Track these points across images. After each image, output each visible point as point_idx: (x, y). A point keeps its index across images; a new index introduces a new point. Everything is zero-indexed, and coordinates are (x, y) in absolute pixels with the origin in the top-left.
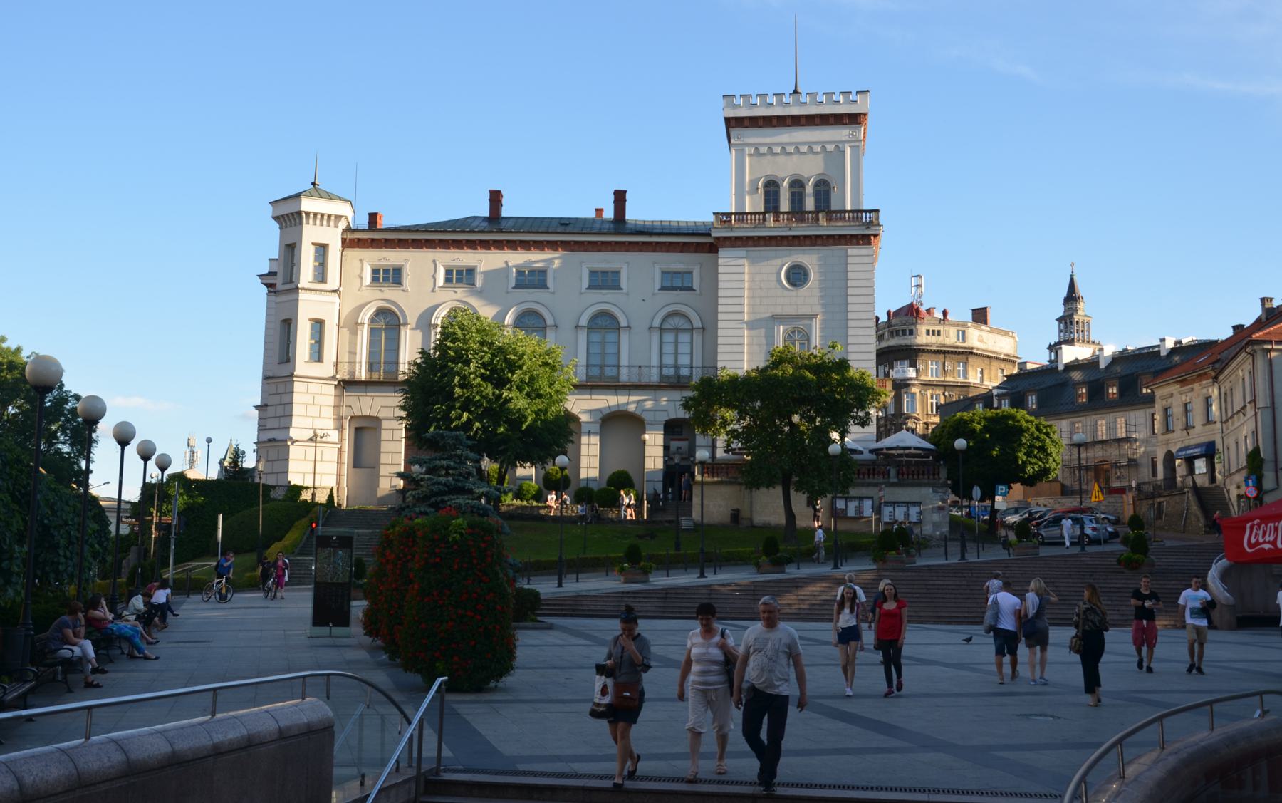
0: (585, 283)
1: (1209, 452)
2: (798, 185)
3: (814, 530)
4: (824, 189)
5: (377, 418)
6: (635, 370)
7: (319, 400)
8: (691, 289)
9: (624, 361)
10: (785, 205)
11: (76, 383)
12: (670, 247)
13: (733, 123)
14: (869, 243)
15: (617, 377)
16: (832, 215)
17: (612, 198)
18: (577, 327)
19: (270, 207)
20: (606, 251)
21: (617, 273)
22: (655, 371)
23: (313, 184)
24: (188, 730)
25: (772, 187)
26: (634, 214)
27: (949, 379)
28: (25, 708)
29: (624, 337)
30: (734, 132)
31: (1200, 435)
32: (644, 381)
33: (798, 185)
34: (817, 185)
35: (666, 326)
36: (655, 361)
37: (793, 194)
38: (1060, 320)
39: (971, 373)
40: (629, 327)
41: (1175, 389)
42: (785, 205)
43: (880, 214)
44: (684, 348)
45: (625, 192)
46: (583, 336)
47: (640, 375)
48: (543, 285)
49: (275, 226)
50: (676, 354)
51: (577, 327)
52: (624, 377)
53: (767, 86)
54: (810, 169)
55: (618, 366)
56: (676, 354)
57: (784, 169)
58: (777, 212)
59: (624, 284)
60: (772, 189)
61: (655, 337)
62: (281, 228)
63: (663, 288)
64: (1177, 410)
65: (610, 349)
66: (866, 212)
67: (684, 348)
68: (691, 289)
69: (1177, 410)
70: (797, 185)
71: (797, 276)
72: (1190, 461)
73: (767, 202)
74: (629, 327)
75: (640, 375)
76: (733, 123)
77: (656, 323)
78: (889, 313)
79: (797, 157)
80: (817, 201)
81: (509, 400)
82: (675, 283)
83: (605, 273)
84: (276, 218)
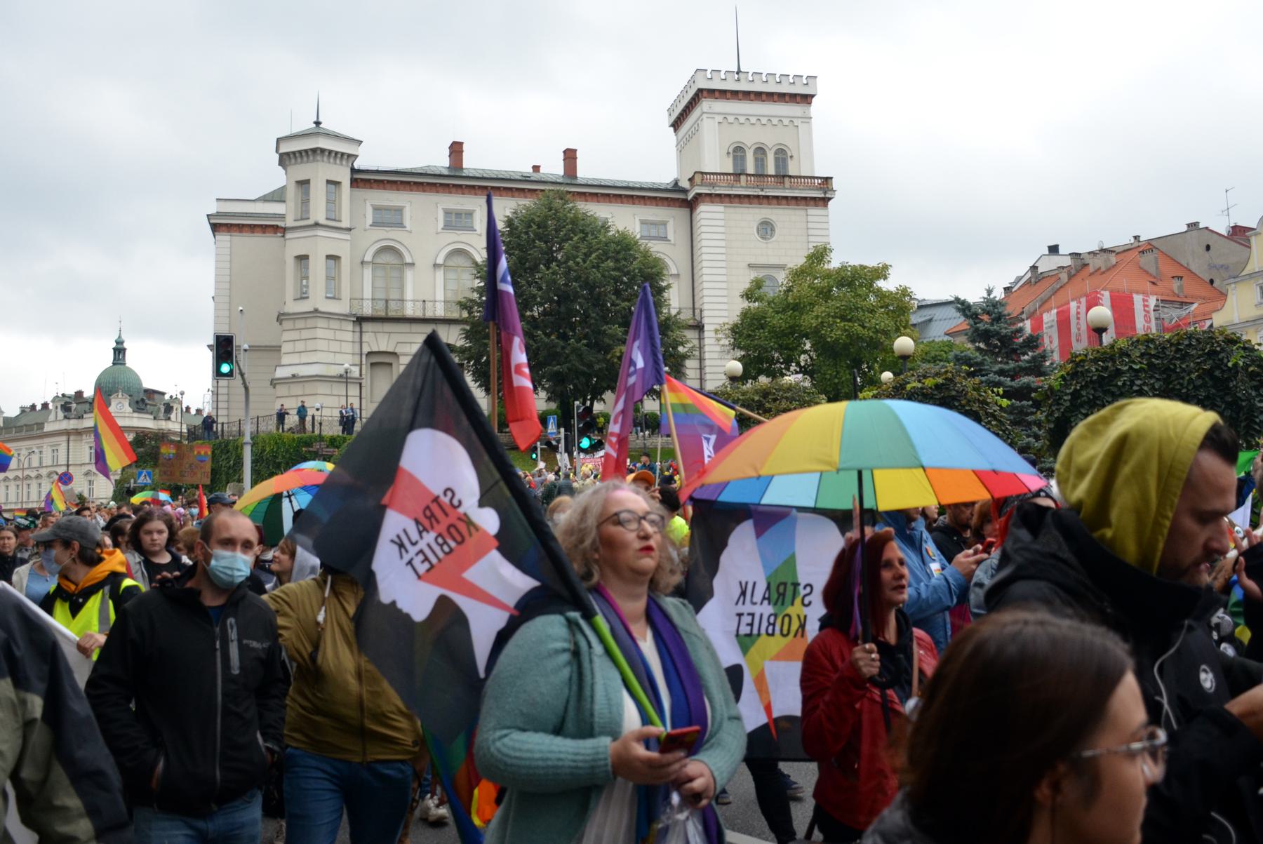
0: (441, 224)
3: (1047, 431)
4: (782, 156)
5: (394, 354)
7: (340, 335)
8: (665, 239)
9: (409, 295)
12: (643, 200)
16: (782, 177)
17: (562, 156)
18: (363, 263)
20: (431, 191)
24: (1064, 546)
25: (738, 152)
26: (585, 171)
29: (409, 274)
32: (429, 314)
45: (461, 144)
46: (368, 272)
47: (424, 309)
51: (363, 263)
54: (770, 139)
55: (402, 300)
57: (750, 138)
59: (407, 222)
60: (780, 156)
65: (380, 283)
68: (665, 239)
70: (760, 151)
71: (766, 229)
73: (735, 165)
75: (424, 309)
79: (759, 127)
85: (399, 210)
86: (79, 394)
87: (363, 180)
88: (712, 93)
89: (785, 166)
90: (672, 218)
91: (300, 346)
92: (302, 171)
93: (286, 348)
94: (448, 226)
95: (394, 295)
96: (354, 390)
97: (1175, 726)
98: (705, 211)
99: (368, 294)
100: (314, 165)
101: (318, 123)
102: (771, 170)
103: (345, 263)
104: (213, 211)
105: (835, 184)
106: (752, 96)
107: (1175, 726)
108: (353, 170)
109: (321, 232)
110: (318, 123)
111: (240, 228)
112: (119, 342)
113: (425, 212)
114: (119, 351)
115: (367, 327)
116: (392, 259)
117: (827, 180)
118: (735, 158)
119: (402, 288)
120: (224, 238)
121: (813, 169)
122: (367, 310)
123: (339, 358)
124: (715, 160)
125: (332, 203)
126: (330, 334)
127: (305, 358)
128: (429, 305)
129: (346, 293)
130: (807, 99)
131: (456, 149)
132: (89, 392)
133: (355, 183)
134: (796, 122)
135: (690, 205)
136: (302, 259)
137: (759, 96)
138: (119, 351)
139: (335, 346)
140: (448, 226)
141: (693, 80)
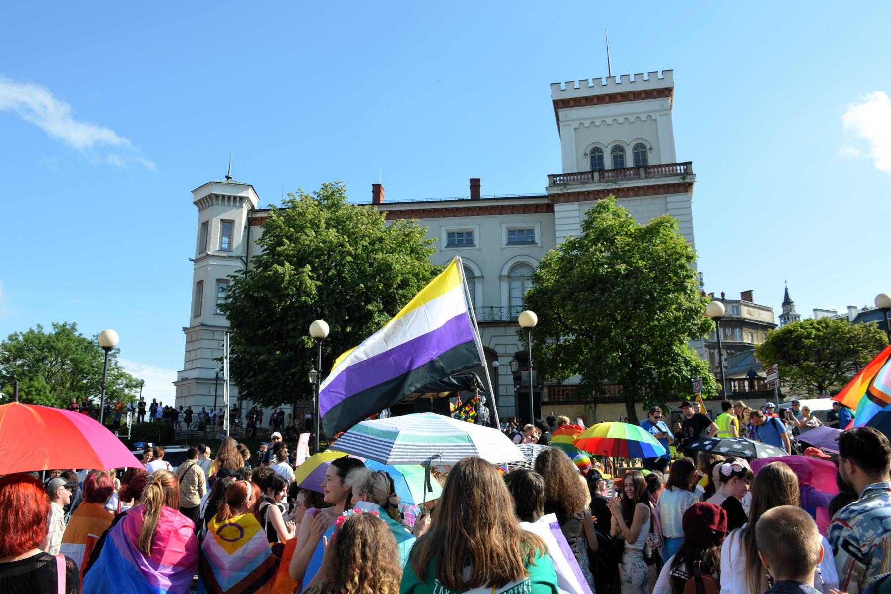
0: (505, 240)
2: (618, 151)
4: (641, 151)
6: (488, 310)
8: (533, 242)
11: (87, 331)
13: (560, 104)
14: (686, 191)
16: (642, 165)
19: (192, 195)
21: (531, 231)
22: (505, 311)
23: (228, 177)
25: (596, 156)
26: (485, 192)
27: (730, 341)
28: (55, 574)
30: (563, 113)
33: (618, 151)
34: (635, 148)
36: (505, 302)
37: (615, 157)
39: (745, 336)
40: (482, 277)
43: (693, 165)
47: (492, 314)
53: (586, 70)
54: (628, 138)
57: (606, 140)
58: (602, 171)
60: (597, 154)
61: (505, 285)
62: (200, 211)
66: (680, 164)
73: (593, 164)
74: (482, 277)
75: (492, 314)
76: (560, 104)
77: (505, 272)
78: (81, 335)
79: (614, 128)
81: (91, 401)
83: (521, 232)
84: (195, 203)
89: (645, 160)
106: (583, 102)
109: (212, 262)
118: (593, 159)
121: (675, 159)
128: (496, 310)
130: (665, 92)
131: (475, 184)
137: (612, 98)
140: (510, 243)
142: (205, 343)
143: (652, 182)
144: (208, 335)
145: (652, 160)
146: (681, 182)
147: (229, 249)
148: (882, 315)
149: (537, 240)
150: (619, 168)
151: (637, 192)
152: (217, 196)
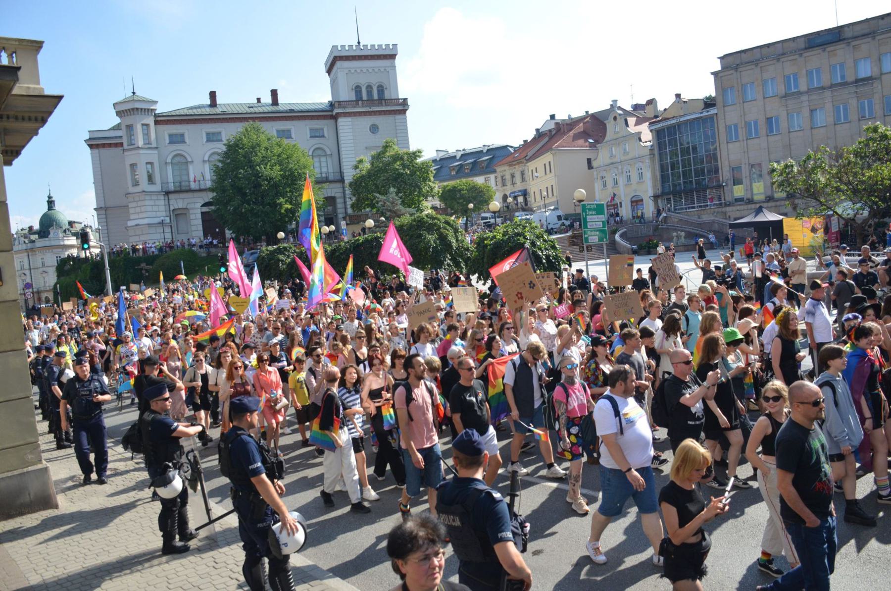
0: (205, 139)
1: (525, 194)
2: (369, 88)
4: (381, 89)
5: (186, 209)
7: (157, 202)
8: (323, 136)
9: (192, 179)
10: (365, 97)
15: (189, 186)
16: (382, 100)
25: (358, 89)
26: (284, 99)
29: (191, 167)
31: (519, 186)
32: (203, 187)
35: (174, 161)
37: (368, 92)
38: (525, 141)
41: (506, 168)
42: (365, 97)
44: (324, 164)
48: (714, 105)
49: (404, 89)
50: (321, 167)
52: (193, 186)
54: (374, 81)
56: (321, 167)
57: (363, 81)
59: (187, 140)
63: (311, 137)
64: (508, 177)
67: (324, 164)
68: (323, 136)
69: (508, 177)
70: (369, 88)
71: (374, 129)
72: (515, 198)
73: (356, 96)
77: (206, 158)
80: (379, 94)
82: (316, 134)
85: (182, 135)
86: (31, 228)
87: (162, 120)
88: (341, 58)
90: (326, 126)
91: (138, 210)
92: (129, 120)
93: (131, 205)
94: (208, 140)
95: (185, 178)
96: (168, 230)
97: (541, 464)
98: (341, 120)
99: (171, 179)
100: (133, 116)
101: (134, 93)
102: (376, 96)
103: (156, 165)
104: (88, 137)
105: (409, 103)
107: (541, 464)
108: (156, 116)
109: (141, 151)
110: (134, 93)
111: (104, 146)
112: (50, 197)
113: (195, 135)
114: (51, 203)
115: (171, 196)
116: (181, 162)
117: (405, 100)
118: (356, 92)
119: (188, 175)
120: (96, 151)
122: (171, 187)
123: (159, 214)
124: (347, 95)
125: (147, 135)
126: (152, 203)
127: (141, 216)
129: (157, 178)
130: (392, 57)
132: (37, 227)
133: (157, 123)
134: (388, 69)
135: (335, 118)
136: (133, 166)
138: (51, 203)
139: (155, 208)
140: (208, 140)
141: (331, 52)
142: (147, 203)
143: (389, 108)
144: (148, 198)
145: (387, 96)
146: (402, 107)
147: (149, 143)
148: (338, 177)
149: (326, 135)
150: (370, 101)
151: (380, 113)
152: (137, 109)
